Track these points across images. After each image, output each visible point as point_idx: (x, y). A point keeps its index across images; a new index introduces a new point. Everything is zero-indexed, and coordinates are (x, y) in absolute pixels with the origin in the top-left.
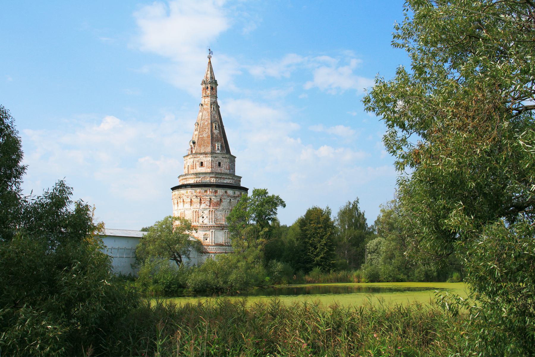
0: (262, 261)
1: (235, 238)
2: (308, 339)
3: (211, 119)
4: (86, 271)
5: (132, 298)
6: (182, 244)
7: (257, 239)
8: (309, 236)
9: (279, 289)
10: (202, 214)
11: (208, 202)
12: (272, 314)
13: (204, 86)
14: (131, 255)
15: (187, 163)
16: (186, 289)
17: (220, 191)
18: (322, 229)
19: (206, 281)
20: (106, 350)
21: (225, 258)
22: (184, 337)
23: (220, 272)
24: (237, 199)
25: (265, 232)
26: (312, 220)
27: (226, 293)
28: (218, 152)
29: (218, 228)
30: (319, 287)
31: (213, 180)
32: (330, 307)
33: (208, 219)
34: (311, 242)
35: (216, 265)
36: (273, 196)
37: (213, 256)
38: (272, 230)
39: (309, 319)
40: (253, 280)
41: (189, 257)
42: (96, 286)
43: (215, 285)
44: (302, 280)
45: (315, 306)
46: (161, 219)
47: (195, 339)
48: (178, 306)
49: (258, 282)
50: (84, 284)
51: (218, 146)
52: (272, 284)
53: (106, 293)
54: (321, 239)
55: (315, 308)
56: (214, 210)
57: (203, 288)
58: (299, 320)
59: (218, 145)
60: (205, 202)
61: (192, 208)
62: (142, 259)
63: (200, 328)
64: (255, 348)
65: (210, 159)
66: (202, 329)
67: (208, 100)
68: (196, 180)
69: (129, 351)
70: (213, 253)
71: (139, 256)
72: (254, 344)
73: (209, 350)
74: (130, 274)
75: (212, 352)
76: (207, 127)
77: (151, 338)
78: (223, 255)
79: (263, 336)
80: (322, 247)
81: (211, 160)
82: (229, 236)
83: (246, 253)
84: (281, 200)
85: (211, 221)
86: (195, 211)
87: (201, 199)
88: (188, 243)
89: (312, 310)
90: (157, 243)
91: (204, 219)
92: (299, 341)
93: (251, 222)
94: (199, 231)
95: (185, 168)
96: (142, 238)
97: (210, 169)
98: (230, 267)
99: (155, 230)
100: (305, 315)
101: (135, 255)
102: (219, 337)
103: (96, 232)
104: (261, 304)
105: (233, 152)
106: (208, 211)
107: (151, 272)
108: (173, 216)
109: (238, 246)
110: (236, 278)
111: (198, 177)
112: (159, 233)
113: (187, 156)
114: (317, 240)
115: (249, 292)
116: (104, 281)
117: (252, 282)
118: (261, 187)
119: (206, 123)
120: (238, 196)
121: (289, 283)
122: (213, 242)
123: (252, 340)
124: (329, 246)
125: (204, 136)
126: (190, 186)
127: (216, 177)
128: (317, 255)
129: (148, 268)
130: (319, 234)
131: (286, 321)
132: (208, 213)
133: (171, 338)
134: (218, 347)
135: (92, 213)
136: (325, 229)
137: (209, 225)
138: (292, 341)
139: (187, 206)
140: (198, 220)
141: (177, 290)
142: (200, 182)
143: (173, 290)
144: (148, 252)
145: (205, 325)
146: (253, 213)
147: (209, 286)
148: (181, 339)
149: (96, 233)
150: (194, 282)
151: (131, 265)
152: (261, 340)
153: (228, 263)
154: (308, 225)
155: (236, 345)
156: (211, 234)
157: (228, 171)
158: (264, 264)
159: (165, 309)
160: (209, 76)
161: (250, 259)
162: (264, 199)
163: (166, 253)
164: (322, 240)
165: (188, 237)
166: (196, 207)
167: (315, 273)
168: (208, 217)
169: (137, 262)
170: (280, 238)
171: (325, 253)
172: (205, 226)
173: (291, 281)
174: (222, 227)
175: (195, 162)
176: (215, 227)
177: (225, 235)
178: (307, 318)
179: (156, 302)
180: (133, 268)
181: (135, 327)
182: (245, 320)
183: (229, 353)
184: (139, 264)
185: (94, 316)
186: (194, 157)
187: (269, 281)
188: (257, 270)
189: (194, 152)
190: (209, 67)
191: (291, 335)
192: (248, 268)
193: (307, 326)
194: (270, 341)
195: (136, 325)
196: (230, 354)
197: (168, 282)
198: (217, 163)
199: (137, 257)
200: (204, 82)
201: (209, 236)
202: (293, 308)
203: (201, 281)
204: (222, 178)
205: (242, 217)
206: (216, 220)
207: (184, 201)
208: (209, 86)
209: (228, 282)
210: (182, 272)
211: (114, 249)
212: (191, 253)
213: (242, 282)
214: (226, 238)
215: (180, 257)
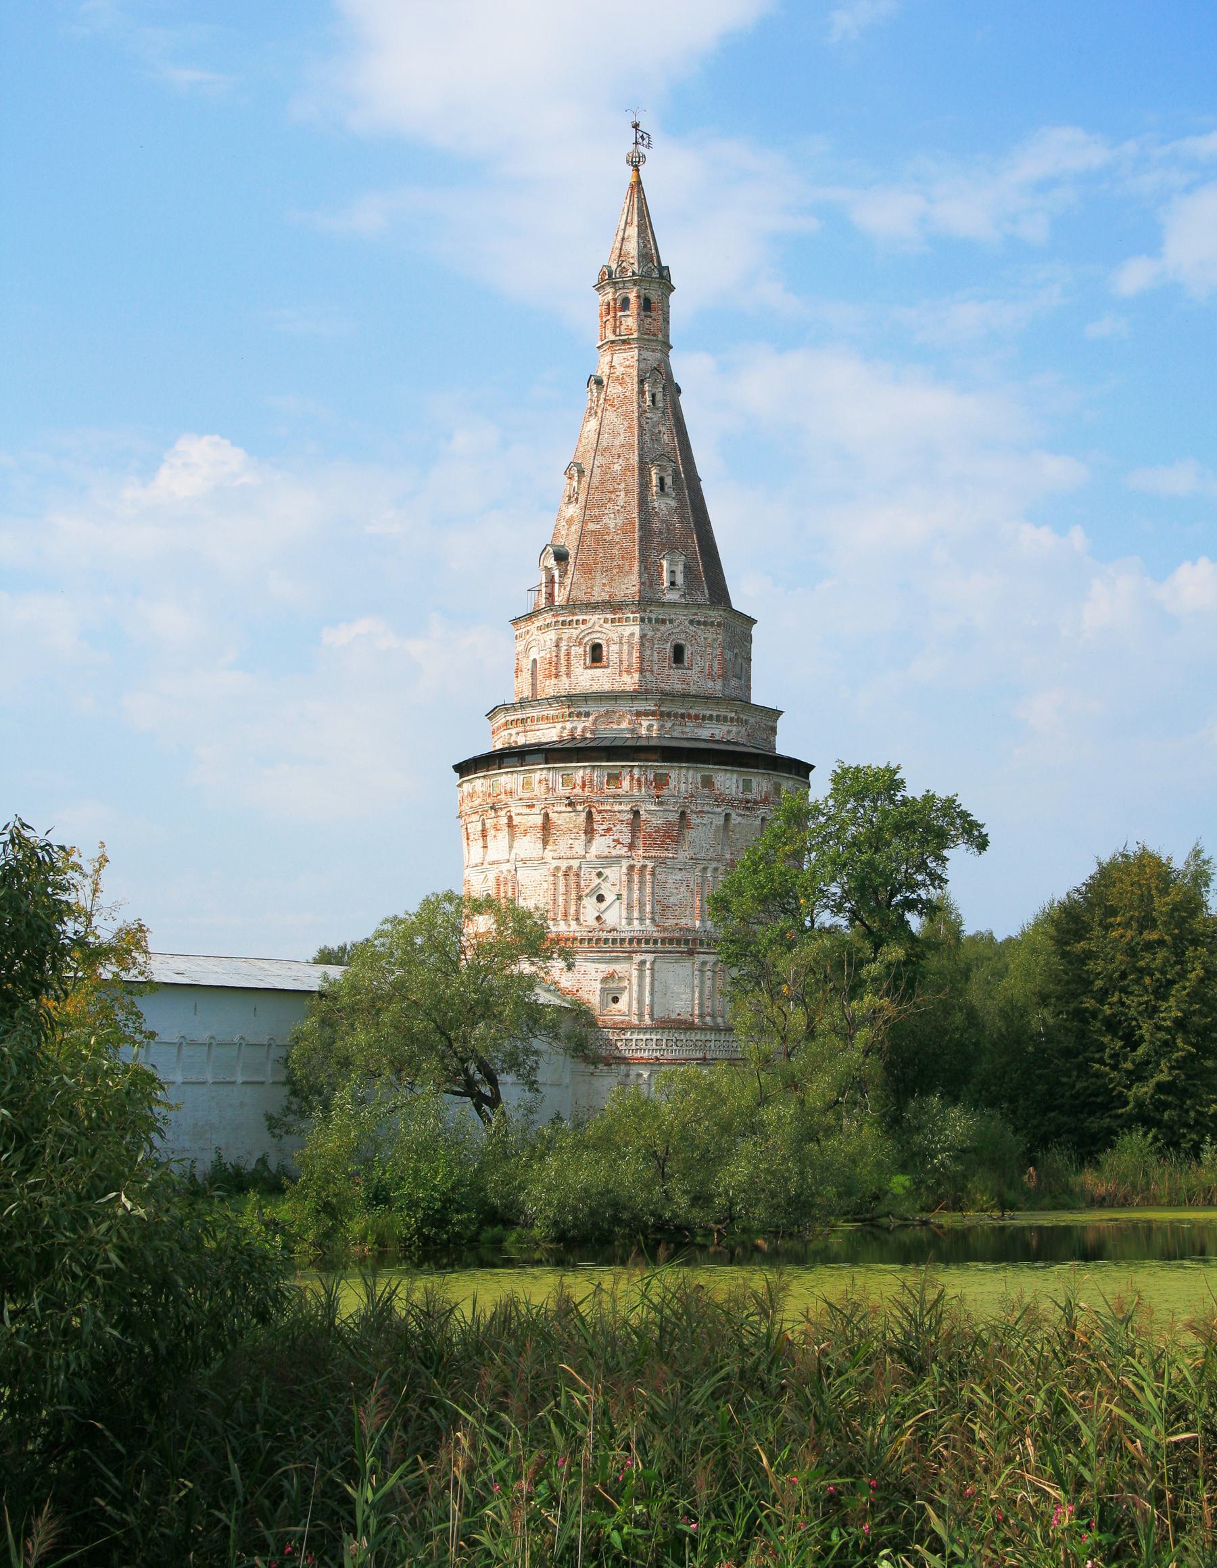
0: (876, 1099)
1: (747, 992)
2: (1081, 1484)
3: (641, 449)
4: (38, 1154)
5: (247, 1274)
6: (500, 1022)
7: (851, 999)
8: (1099, 983)
9: (952, 1230)
10: (597, 881)
11: (626, 829)
12: (904, 1354)
13: (610, 296)
14: (268, 1075)
15: (527, 649)
16: (519, 1229)
17: (682, 779)
18: (1162, 954)
19: (609, 1191)
20: (123, 1524)
21: (696, 1087)
22: (483, 1463)
23: (676, 1153)
24: (761, 812)
25: (889, 966)
26: (1112, 912)
27: (703, 1247)
28: (673, 596)
29: (669, 948)
30: (1150, 1229)
31: (648, 729)
32: (1190, 1326)
33: (624, 906)
34: (1108, 1012)
35: (656, 1117)
36: (929, 798)
37: (645, 1076)
38: (920, 956)
39: (1090, 1384)
40: (831, 1190)
41: (535, 1082)
42: (79, 1221)
43: (652, 1214)
44: (1068, 1190)
45: (1114, 1318)
46: (408, 905)
47: (536, 1472)
48: (465, 1312)
49: (855, 1199)
50: (26, 1210)
51: (673, 572)
52: (922, 1209)
53: (125, 1252)
54: (1157, 999)
55: (1120, 1329)
56: (650, 865)
57: (595, 1224)
58: (1039, 1388)
59: (669, 568)
60: (609, 830)
61: (551, 854)
62: (320, 1093)
63: (559, 1420)
64: (822, 1523)
65: (636, 629)
66: (572, 1427)
67: (626, 361)
68: (569, 725)
69: (227, 1528)
70: (645, 1063)
71: (306, 1077)
72: (815, 1500)
73: (601, 1526)
74: (262, 1161)
75: (616, 1537)
76: (623, 486)
77: (331, 1466)
78: (692, 1069)
79: (859, 1460)
80: (1162, 1035)
81: (637, 636)
82: (719, 983)
83: (798, 1062)
84: (964, 815)
85: (636, 915)
86: (564, 868)
87: (590, 814)
88: (530, 1017)
89: (1100, 1341)
90: (385, 1017)
91: (604, 905)
92: (1038, 1490)
93: (826, 918)
94: (581, 965)
95: (518, 671)
96: (321, 995)
97: (636, 676)
98: (726, 1128)
99: (377, 957)
100: (1069, 1363)
101: (286, 1072)
102: (648, 1464)
103: (109, 967)
104: (856, 1306)
105: (739, 603)
106: (624, 870)
107: (356, 1149)
108: (461, 891)
109: (762, 1031)
110: (752, 1180)
111: (579, 715)
112: (399, 972)
113: (530, 617)
114: (1140, 1004)
115: (812, 1246)
116: (118, 1197)
117: (829, 1200)
118: (872, 758)
119: (617, 467)
120: (765, 801)
121: (1004, 1205)
122: (647, 1010)
123: (807, 1482)
124: (1198, 1034)
125: (606, 527)
126: (541, 757)
127: (662, 714)
128: (1138, 1075)
129: (344, 1130)
130: (1152, 975)
131: (972, 1390)
132: (624, 878)
133: (425, 1467)
134: (642, 1514)
135: (90, 880)
136: (1179, 955)
137: (627, 935)
138: (1001, 1491)
139: (529, 846)
140: (577, 911)
141: (478, 1234)
142: (588, 735)
143: (458, 1235)
144: (347, 1059)
145: (583, 1404)
146: (833, 879)
147: (625, 1216)
148: (469, 1472)
149: (107, 971)
150: (555, 1197)
151: (269, 1118)
152: (853, 1484)
153: (714, 1107)
154: (1098, 931)
155: (732, 1506)
156: (635, 973)
157: (715, 687)
158: (884, 1115)
159: (402, 1326)
160: (632, 247)
161: (820, 1089)
162: (886, 814)
163: (430, 1063)
164: (1165, 1005)
165: (531, 987)
166: (569, 853)
167: (1126, 1157)
168: (625, 897)
169: (294, 1107)
170: (961, 993)
171: (1180, 1065)
172: (610, 936)
173: (1011, 1196)
174: (687, 942)
175: (563, 644)
176: (655, 942)
177: (702, 982)
178: (1078, 1380)
179: (361, 1291)
180: (277, 1131)
181: (261, 1412)
182: (774, 1382)
183: (694, 1543)
184: (303, 1114)
185: (68, 1365)
186: (563, 623)
187: (909, 1192)
188: (849, 1144)
189: (559, 599)
190: (631, 205)
191: (997, 1458)
192: (811, 1135)
193: (1077, 1418)
194: (896, 1488)
195: (261, 1405)
196: (702, 1546)
197: (437, 1195)
198: (668, 647)
199: (294, 1083)
200: (609, 279)
201: (626, 983)
202: (1010, 1330)
203: (586, 1190)
204: (689, 716)
205: (780, 895)
206: (662, 907)
207: (515, 823)
208: (632, 296)
209: (714, 1196)
210: (501, 1152)
211: (193, 1043)
212: (541, 1063)
213: (781, 1199)
214: (707, 991)
215: (492, 1080)
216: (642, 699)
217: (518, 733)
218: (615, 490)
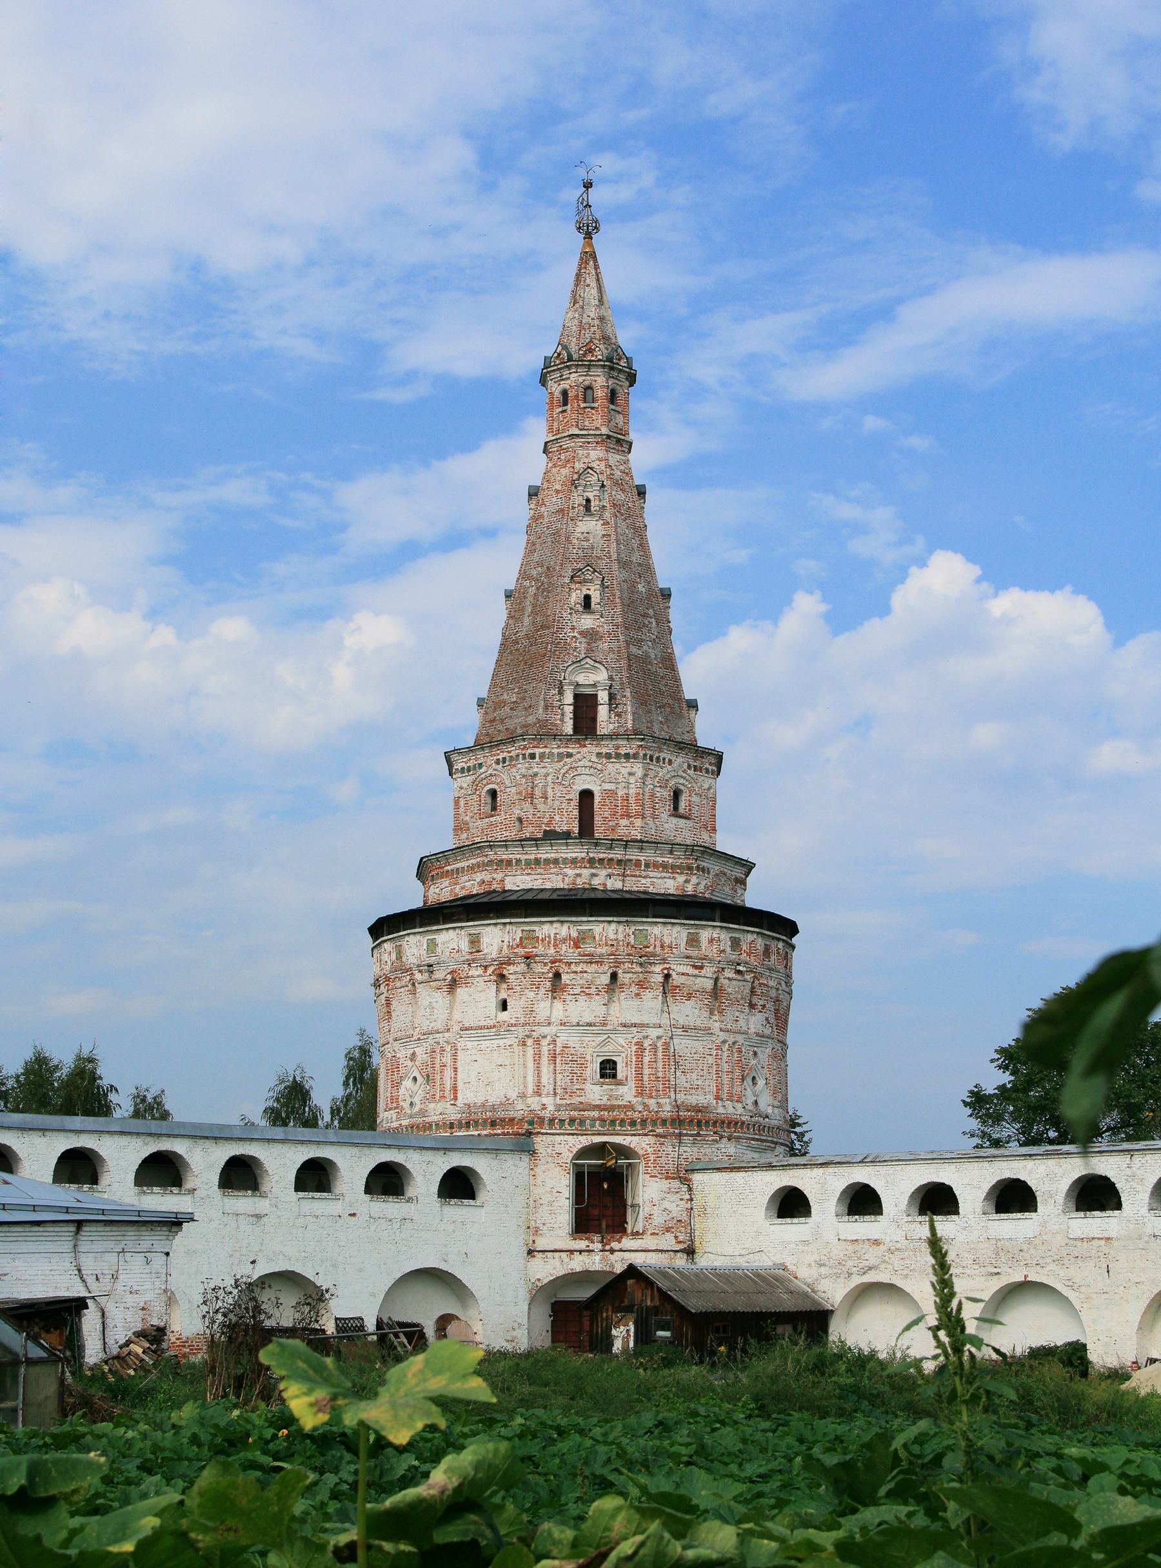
218: (645, 616)
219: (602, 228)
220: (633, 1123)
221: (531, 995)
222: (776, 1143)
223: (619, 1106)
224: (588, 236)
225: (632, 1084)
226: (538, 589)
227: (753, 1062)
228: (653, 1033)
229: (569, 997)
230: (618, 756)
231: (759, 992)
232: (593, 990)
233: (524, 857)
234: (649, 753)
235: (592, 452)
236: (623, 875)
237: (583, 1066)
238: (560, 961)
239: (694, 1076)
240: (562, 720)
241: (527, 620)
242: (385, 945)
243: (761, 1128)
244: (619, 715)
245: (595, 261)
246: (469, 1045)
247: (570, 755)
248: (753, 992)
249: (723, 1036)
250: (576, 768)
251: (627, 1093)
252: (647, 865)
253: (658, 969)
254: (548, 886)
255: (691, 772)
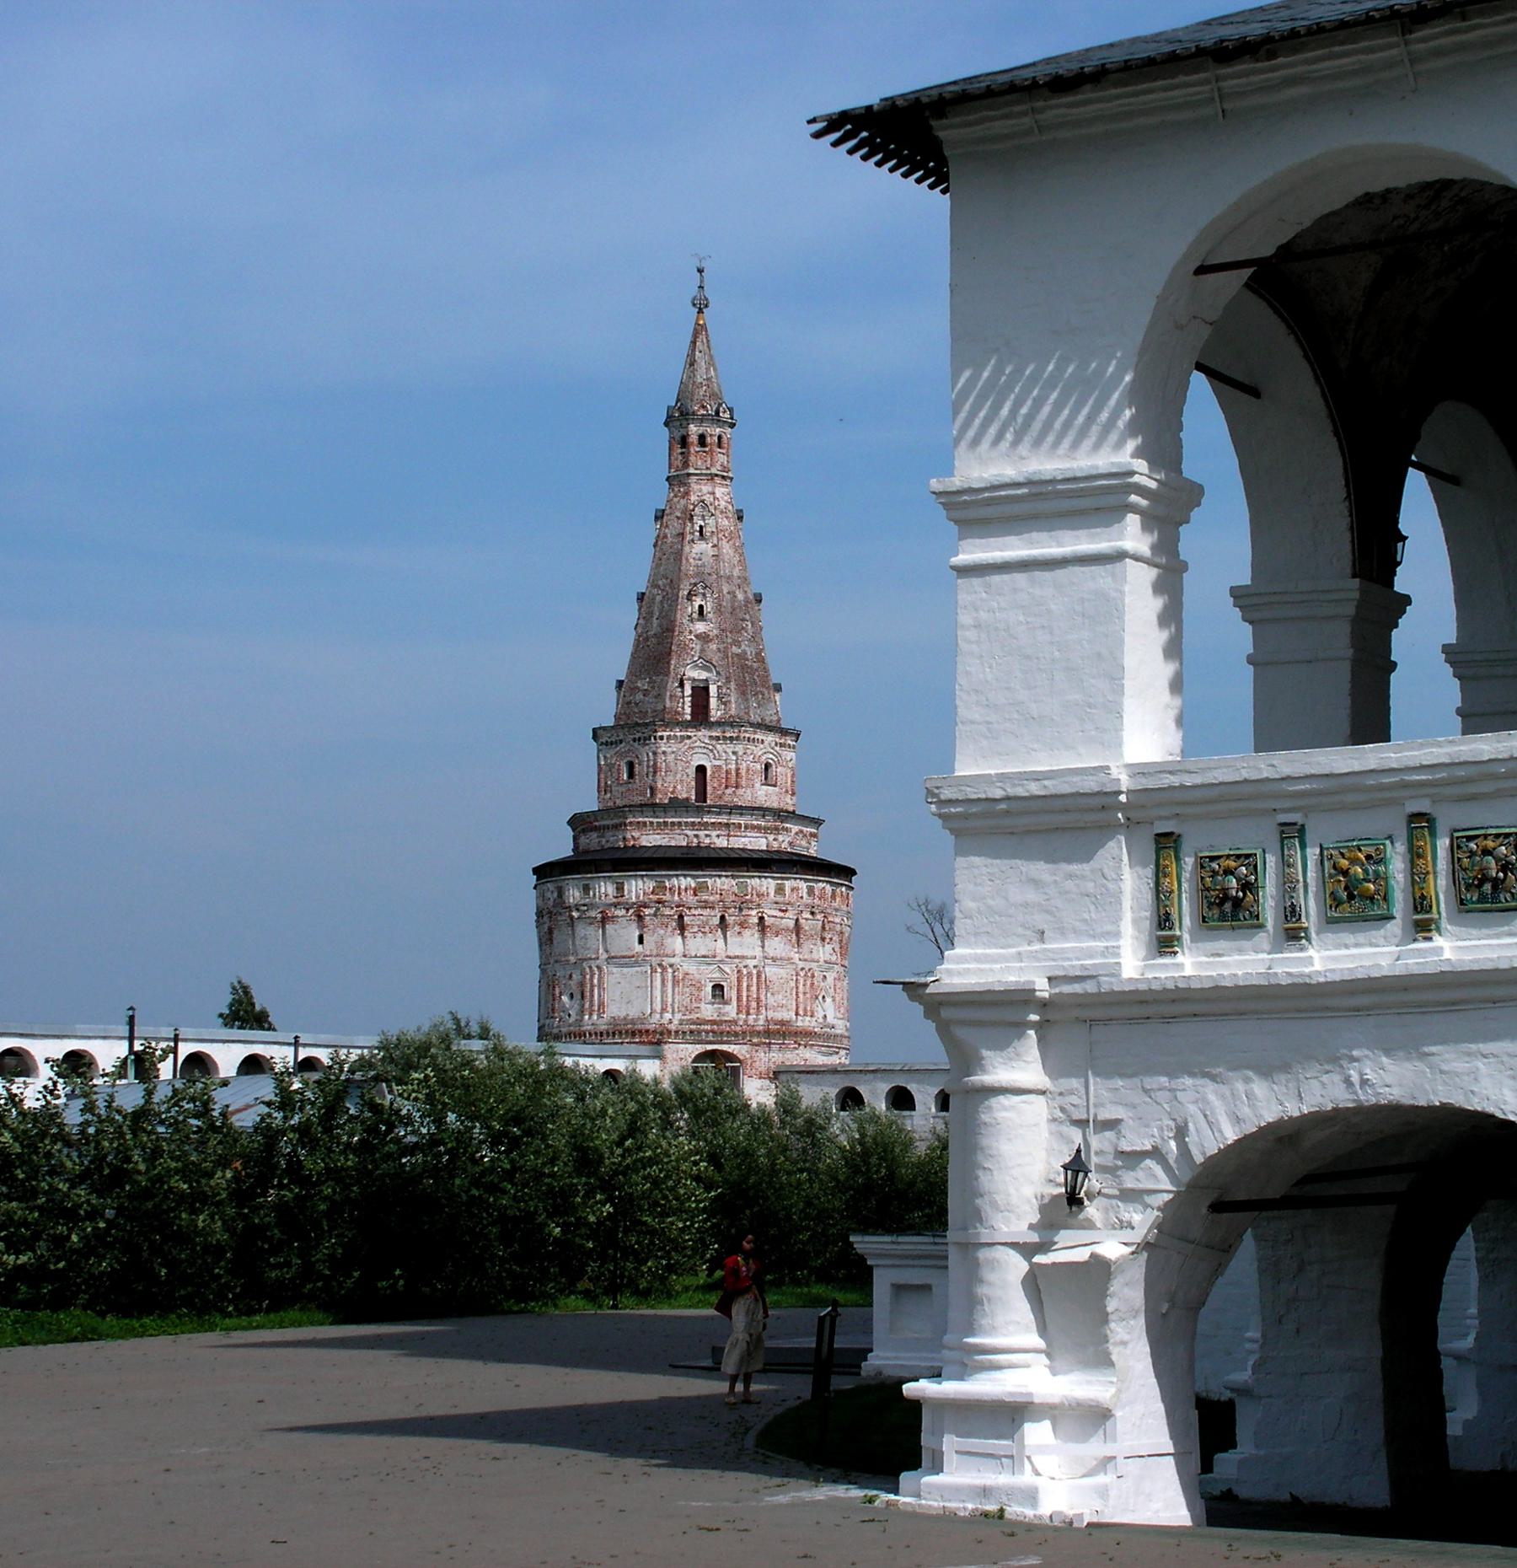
125: (745, 652)
216: (737, 814)
217: (718, 836)
219: (710, 305)
220: (736, 1034)
221: (662, 932)
222: (839, 1048)
223: (726, 1021)
224: (700, 311)
225: (734, 1003)
226: (664, 597)
227: (822, 984)
228: (751, 963)
229: (689, 935)
230: (725, 738)
231: (827, 928)
232: (707, 930)
233: (655, 820)
234: (747, 735)
235: (703, 487)
236: (729, 836)
237: (699, 989)
238: (683, 906)
239: (780, 997)
240: (683, 708)
241: (655, 622)
242: (548, 884)
243: (829, 1037)
244: (725, 704)
245: (706, 331)
246: (615, 970)
247: (689, 737)
248: (823, 928)
249: (801, 965)
250: (693, 748)
251: (731, 1011)
252: (746, 827)
253: (754, 913)
254: (673, 843)
255: (777, 748)
